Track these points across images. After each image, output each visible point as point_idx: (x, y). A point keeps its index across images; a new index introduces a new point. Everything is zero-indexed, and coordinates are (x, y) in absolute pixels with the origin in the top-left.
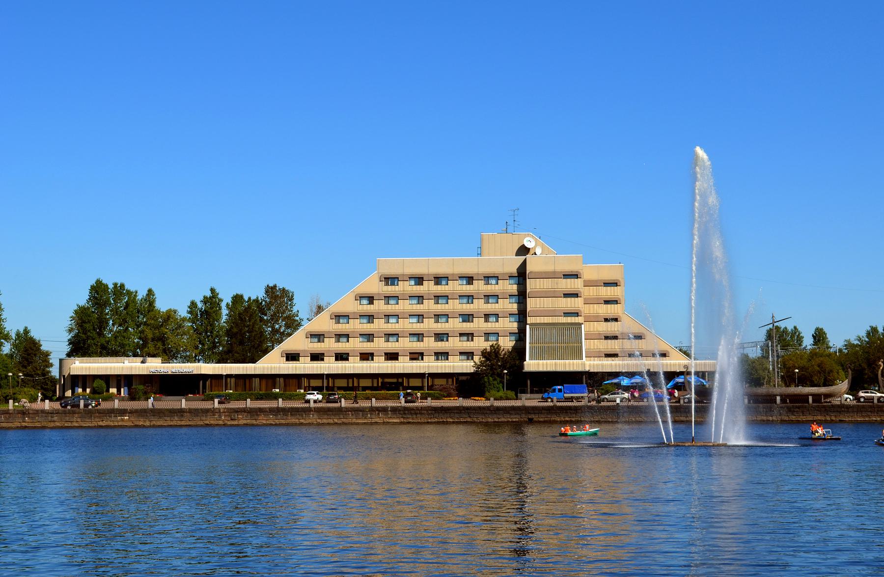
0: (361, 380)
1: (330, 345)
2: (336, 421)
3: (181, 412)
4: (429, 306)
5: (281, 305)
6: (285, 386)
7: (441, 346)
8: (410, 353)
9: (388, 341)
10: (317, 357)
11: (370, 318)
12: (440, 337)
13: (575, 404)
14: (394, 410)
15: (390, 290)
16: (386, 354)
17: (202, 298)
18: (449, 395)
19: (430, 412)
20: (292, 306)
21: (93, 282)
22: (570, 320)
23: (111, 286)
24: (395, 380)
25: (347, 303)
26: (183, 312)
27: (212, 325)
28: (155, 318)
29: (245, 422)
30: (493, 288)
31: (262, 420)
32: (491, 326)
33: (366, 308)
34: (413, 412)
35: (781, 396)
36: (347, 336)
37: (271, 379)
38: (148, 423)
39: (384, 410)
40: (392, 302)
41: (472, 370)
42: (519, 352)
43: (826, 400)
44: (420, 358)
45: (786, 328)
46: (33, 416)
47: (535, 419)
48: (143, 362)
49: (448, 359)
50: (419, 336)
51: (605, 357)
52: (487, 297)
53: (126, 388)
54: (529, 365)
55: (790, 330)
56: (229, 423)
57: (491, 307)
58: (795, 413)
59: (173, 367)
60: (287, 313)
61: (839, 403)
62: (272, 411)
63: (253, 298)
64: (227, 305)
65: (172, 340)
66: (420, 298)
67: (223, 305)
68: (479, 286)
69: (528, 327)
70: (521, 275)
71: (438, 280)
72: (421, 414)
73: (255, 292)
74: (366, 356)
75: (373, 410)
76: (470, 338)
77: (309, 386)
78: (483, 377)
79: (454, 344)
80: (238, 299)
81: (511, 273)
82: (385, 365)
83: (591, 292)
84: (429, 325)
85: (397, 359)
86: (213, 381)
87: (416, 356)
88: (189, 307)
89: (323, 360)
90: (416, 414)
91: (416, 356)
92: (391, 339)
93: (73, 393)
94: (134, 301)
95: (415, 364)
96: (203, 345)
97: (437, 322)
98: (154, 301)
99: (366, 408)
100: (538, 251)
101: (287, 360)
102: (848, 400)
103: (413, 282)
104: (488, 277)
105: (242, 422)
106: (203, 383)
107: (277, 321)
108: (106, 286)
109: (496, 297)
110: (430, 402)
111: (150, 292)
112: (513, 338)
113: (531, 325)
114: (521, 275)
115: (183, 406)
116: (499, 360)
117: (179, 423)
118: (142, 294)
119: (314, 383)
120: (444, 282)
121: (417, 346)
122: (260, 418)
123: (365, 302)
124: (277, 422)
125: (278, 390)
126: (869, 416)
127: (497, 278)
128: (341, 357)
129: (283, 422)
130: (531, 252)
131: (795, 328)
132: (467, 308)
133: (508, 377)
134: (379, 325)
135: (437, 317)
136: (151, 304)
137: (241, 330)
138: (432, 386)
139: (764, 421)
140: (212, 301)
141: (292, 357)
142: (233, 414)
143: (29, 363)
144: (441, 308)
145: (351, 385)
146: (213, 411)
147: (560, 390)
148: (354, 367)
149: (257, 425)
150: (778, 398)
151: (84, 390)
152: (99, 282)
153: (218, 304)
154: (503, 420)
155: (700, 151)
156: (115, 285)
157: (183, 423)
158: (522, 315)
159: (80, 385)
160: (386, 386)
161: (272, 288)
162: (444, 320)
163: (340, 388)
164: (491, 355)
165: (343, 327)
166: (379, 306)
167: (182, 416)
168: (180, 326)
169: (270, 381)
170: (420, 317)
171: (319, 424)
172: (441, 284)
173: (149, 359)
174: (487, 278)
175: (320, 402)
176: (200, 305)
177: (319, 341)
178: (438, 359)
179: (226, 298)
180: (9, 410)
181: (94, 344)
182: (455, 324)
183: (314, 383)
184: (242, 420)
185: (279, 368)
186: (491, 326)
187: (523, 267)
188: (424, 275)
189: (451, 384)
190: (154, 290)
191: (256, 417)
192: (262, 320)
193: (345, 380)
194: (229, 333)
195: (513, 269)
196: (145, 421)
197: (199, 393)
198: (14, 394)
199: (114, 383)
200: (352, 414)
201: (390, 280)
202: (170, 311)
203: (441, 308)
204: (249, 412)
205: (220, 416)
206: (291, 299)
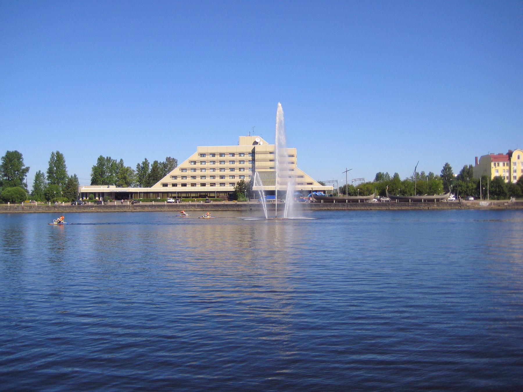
0: (191, 194)
1: (179, 180)
2: (175, 210)
3: (115, 206)
7: (222, 181)
8: (210, 183)
9: (183, 179)
10: (174, 185)
11: (195, 170)
12: (222, 177)
14: (198, 206)
15: (203, 159)
19: (212, 206)
21: (99, 157)
22: (272, 170)
23: (106, 158)
24: (204, 194)
26: (134, 168)
29: (139, 210)
30: (242, 158)
31: (146, 209)
32: (242, 173)
33: (193, 166)
34: (205, 206)
35: (348, 200)
36: (186, 177)
37: (157, 193)
38: (102, 211)
39: (194, 206)
40: (203, 163)
41: (234, 190)
43: (366, 201)
44: (214, 185)
45: (383, 173)
46: (59, 208)
48: (108, 187)
49: (225, 186)
50: (213, 177)
51: (298, 184)
52: (240, 161)
53: (102, 197)
55: (385, 174)
56: (133, 211)
58: (353, 206)
59: (119, 189)
61: (370, 202)
62: (150, 206)
64: (152, 165)
65: (129, 179)
66: (214, 162)
67: (150, 165)
70: (253, 153)
71: (221, 155)
74: (193, 185)
75: (190, 205)
76: (233, 177)
78: (237, 193)
79: (227, 180)
80: (156, 162)
81: (249, 152)
82: (182, 188)
84: (218, 172)
86: (135, 194)
87: (212, 185)
88: (137, 166)
91: (212, 185)
93: (82, 199)
94: (115, 164)
95: (212, 187)
100: (261, 143)
101: (163, 186)
102: (375, 201)
103: (211, 156)
105: (138, 210)
106: (131, 195)
108: (104, 158)
110: (212, 203)
111: (121, 160)
114: (253, 153)
115: (116, 204)
117: (114, 211)
118: (118, 161)
119: (174, 195)
120: (223, 156)
121: (213, 181)
122: (146, 209)
123: (193, 163)
124: (152, 210)
125: (159, 198)
126: (381, 207)
127: (244, 154)
128: (184, 185)
129: (154, 210)
130: (259, 143)
131: (387, 173)
132: (232, 166)
134: (198, 173)
136: (122, 165)
137: (153, 175)
138: (219, 196)
139: (341, 209)
140: (146, 163)
141: (165, 185)
142: (135, 207)
143: (69, 188)
144: (222, 166)
145: (187, 196)
148: (188, 189)
150: (347, 201)
151: (86, 198)
152: (101, 157)
153: (148, 165)
155: (280, 105)
156: (107, 158)
157: (115, 211)
159: (85, 196)
160: (201, 196)
161: (169, 158)
162: (223, 170)
163: (183, 197)
164: (241, 184)
165: (184, 174)
166: (198, 165)
167: (115, 208)
169: (157, 194)
170: (214, 169)
171: (168, 211)
173: (110, 186)
174: (240, 154)
175: (173, 202)
176: (141, 165)
177: (175, 179)
178: (221, 186)
179: (151, 162)
180: (49, 206)
181: (99, 180)
182: (228, 172)
185: (160, 189)
186: (242, 173)
188: (216, 153)
189: (226, 195)
191: (144, 208)
195: (250, 151)
196: (101, 210)
197: (129, 199)
198: (57, 200)
199: (97, 195)
201: (203, 155)
202: (128, 167)
203: (222, 166)
204: (141, 207)
205: (130, 208)
206: (176, 162)
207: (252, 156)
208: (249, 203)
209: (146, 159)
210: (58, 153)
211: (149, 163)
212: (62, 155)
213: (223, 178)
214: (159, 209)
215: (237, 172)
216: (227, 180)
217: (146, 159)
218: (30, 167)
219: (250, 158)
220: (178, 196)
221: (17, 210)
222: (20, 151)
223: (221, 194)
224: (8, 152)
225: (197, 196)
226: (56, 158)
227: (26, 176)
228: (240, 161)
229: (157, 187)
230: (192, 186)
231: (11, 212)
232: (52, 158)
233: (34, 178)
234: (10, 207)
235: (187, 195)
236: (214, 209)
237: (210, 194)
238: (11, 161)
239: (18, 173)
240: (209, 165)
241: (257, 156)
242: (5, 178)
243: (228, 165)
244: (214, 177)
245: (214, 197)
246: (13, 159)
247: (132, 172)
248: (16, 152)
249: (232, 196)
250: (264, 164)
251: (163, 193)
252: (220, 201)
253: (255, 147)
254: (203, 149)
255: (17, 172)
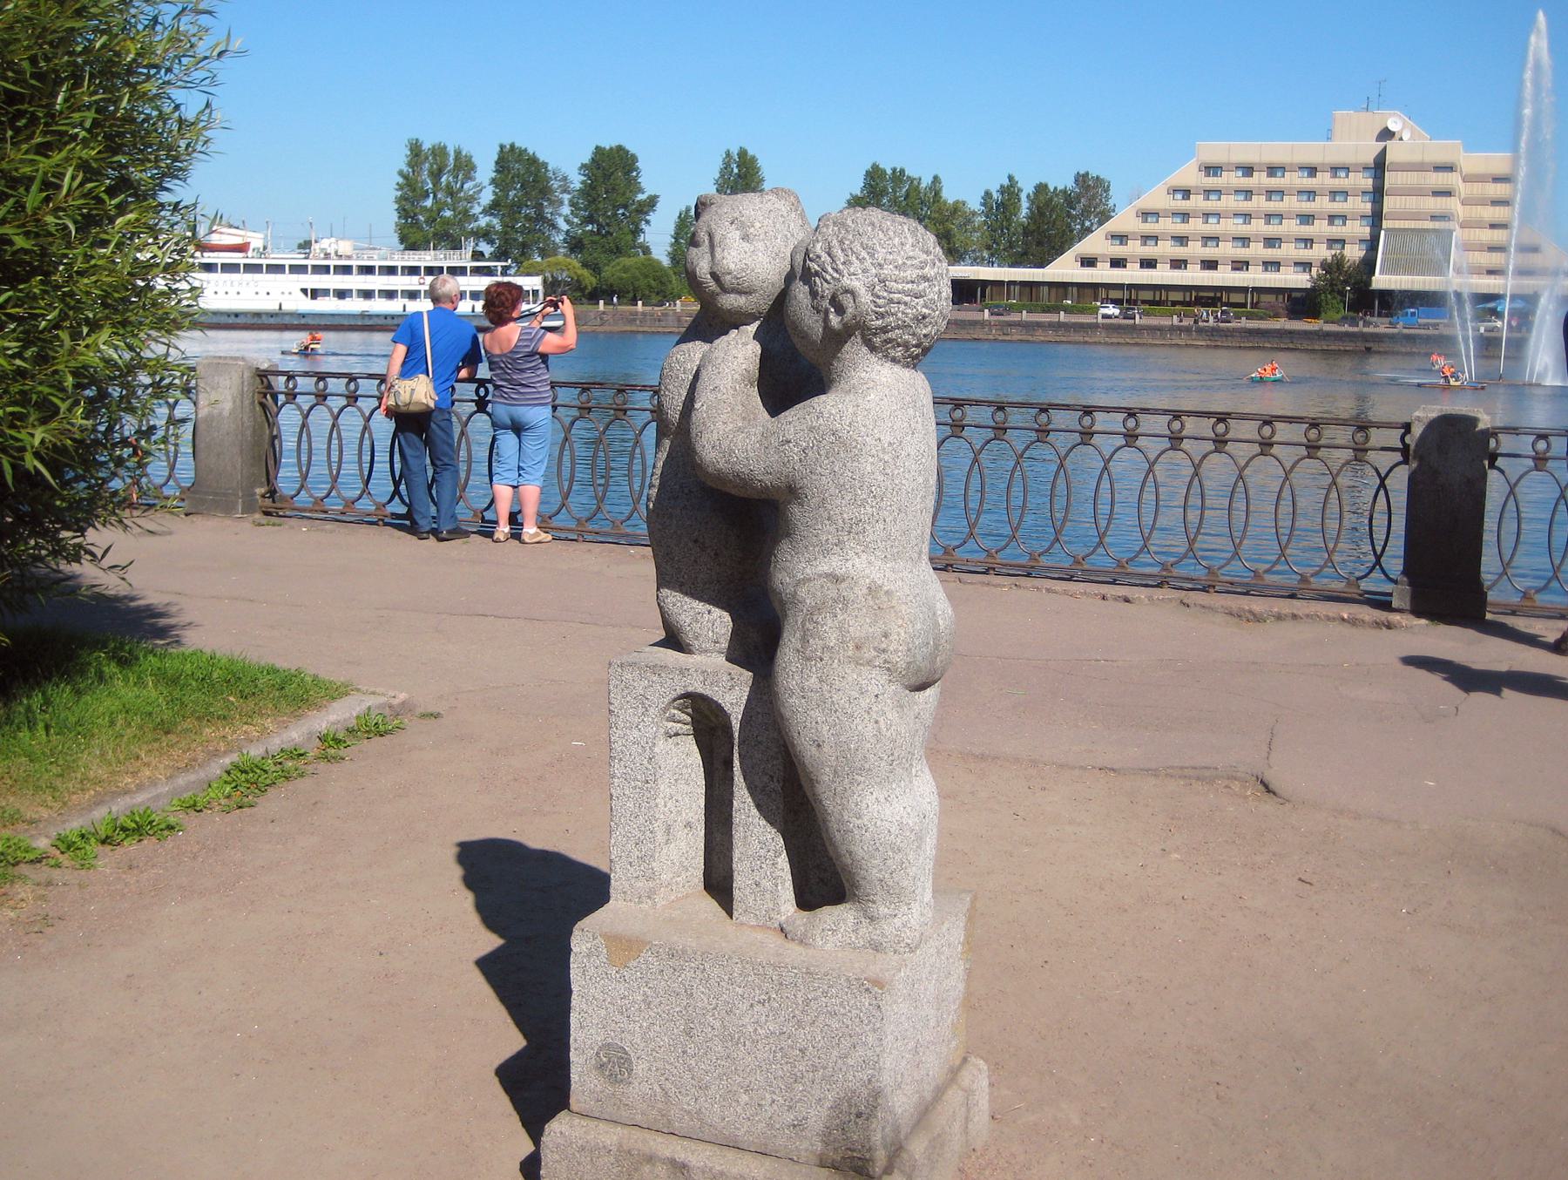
0: (1231, 295)
1: (1135, 249)
4: (1259, 203)
5: (1093, 197)
6: (1078, 297)
7: (1271, 254)
10: (1117, 263)
12: (1271, 242)
13: (1431, 332)
15: (1212, 182)
16: (1202, 262)
17: (999, 187)
18: (1277, 316)
20: (1107, 198)
21: (869, 167)
23: (889, 172)
24: (1212, 294)
25: (1157, 198)
26: (974, 204)
27: (1009, 220)
28: (940, 211)
29: (1020, 337)
30: (1342, 182)
31: (1040, 336)
33: (1181, 204)
34: (1222, 333)
36: (1156, 238)
41: (1309, 285)
42: (1368, 265)
47: (1374, 349)
54: (1377, 281)
57: (1338, 207)
60: (1102, 208)
62: (1051, 325)
63: (1060, 187)
64: (1028, 196)
67: (1023, 196)
68: (1324, 180)
69: (1383, 233)
70: (1379, 167)
71: (1272, 170)
72: (1232, 336)
73: (1061, 180)
74: (1178, 264)
75: (1172, 329)
77: (1107, 298)
80: (1041, 188)
83: (1477, 189)
84: (1258, 227)
85: (1155, 267)
87: (1240, 265)
89: (1125, 266)
90: (1226, 336)
91: (1240, 265)
92: (1209, 243)
94: (917, 189)
96: (998, 244)
97: (1268, 223)
98: (941, 189)
99: (1166, 326)
100: (1406, 136)
101: (1082, 265)
103: (1240, 173)
104: (1336, 168)
105: (1016, 337)
107: (1087, 218)
109: (1345, 193)
110: (1244, 323)
111: (936, 179)
112: (1364, 247)
113: (1387, 230)
114: (1379, 167)
116: (1340, 274)
118: (926, 182)
119: (1114, 294)
120: (1279, 174)
121: (1241, 253)
123: (1179, 196)
124: (1058, 339)
127: (1347, 169)
128: (1149, 263)
129: (1064, 339)
132: (1306, 207)
133: (1351, 296)
134: (1196, 226)
135: (1269, 217)
136: (937, 194)
137: (1039, 228)
138: (1257, 303)
140: (1010, 191)
141: (1088, 262)
144: (1274, 206)
145: (1157, 298)
146: (982, 324)
147: (1413, 314)
149: (1033, 342)
152: (875, 168)
154: (1333, 347)
155: (1541, 16)
156: (894, 170)
158: (1376, 218)
161: (1083, 176)
163: (1144, 302)
164: (1333, 268)
165: (1150, 227)
166: (1197, 202)
168: (969, 221)
169: (1061, 290)
170: (1247, 217)
171: (1106, 343)
172: (1275, 177)
174: (1335, 170)
175: (1116, 317)
176: (995, 195)
177: (1121, 244)
178: (1266, 270)
179: (1027, 188)
182: (1291, 227)
183: (1114, 294)
184: (1016, 334)
186: (1337, 231)
187: (1382, 157)
190: (941, 176)
192: (1069, 215)
193: (1182, 293)
194: (1026, 232)
195: (1369, 159)
197: (976, 302)
200: (1148, 334)
201: (1212, 169)
202: (957, 202)
203: (1274, 206)
206: (1107, 190)
207: (1375, 178)
208: (1324, 329)
209: (1011, 178)
210: (743, 153)
211: (1020, 190)
212: (753, 159)
213: (1275, 247)
214: (1078, 338)
215: (1321, 228)
216: (1289, 251)
217: (1011, 178)
218: (658, 197)
219: (1368, 183)
220: (1129, 296)
221: (663, 324)
222: (632, 148)
223: (1266, 298)
224: (599, 150)
225: (1188, 299)
226: (736, 171)
227: (648, 222)
228: (1334, 194)
229: (1064, 269)
230: (1175, 268)
231: (646, 329)
232: (726, 168)
233: (671, 229)
234: (644, 314)
235: (1158, 297)
236: (1251, 345)
237: (1231, 295)
238: (607, 177)
239: (623, 214)
240: (1230, 202)
241: (1391, 179)
242: (589, 228)
243: (1292, 203)
244: (1247, 241)
245: (1244, 305)
246: (612, 173)
247: (969, 218)
248: (620, 148)
249: (1302, 304)
250: (1411, 203)
251: (1081, 286)
252: (1261, 318)
253: (1385, 147)
254: (1215, 151)
255: (621, 211)
